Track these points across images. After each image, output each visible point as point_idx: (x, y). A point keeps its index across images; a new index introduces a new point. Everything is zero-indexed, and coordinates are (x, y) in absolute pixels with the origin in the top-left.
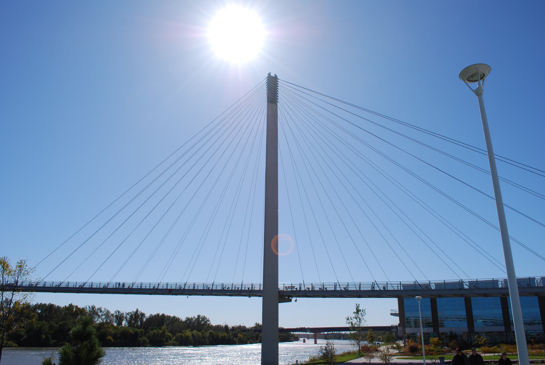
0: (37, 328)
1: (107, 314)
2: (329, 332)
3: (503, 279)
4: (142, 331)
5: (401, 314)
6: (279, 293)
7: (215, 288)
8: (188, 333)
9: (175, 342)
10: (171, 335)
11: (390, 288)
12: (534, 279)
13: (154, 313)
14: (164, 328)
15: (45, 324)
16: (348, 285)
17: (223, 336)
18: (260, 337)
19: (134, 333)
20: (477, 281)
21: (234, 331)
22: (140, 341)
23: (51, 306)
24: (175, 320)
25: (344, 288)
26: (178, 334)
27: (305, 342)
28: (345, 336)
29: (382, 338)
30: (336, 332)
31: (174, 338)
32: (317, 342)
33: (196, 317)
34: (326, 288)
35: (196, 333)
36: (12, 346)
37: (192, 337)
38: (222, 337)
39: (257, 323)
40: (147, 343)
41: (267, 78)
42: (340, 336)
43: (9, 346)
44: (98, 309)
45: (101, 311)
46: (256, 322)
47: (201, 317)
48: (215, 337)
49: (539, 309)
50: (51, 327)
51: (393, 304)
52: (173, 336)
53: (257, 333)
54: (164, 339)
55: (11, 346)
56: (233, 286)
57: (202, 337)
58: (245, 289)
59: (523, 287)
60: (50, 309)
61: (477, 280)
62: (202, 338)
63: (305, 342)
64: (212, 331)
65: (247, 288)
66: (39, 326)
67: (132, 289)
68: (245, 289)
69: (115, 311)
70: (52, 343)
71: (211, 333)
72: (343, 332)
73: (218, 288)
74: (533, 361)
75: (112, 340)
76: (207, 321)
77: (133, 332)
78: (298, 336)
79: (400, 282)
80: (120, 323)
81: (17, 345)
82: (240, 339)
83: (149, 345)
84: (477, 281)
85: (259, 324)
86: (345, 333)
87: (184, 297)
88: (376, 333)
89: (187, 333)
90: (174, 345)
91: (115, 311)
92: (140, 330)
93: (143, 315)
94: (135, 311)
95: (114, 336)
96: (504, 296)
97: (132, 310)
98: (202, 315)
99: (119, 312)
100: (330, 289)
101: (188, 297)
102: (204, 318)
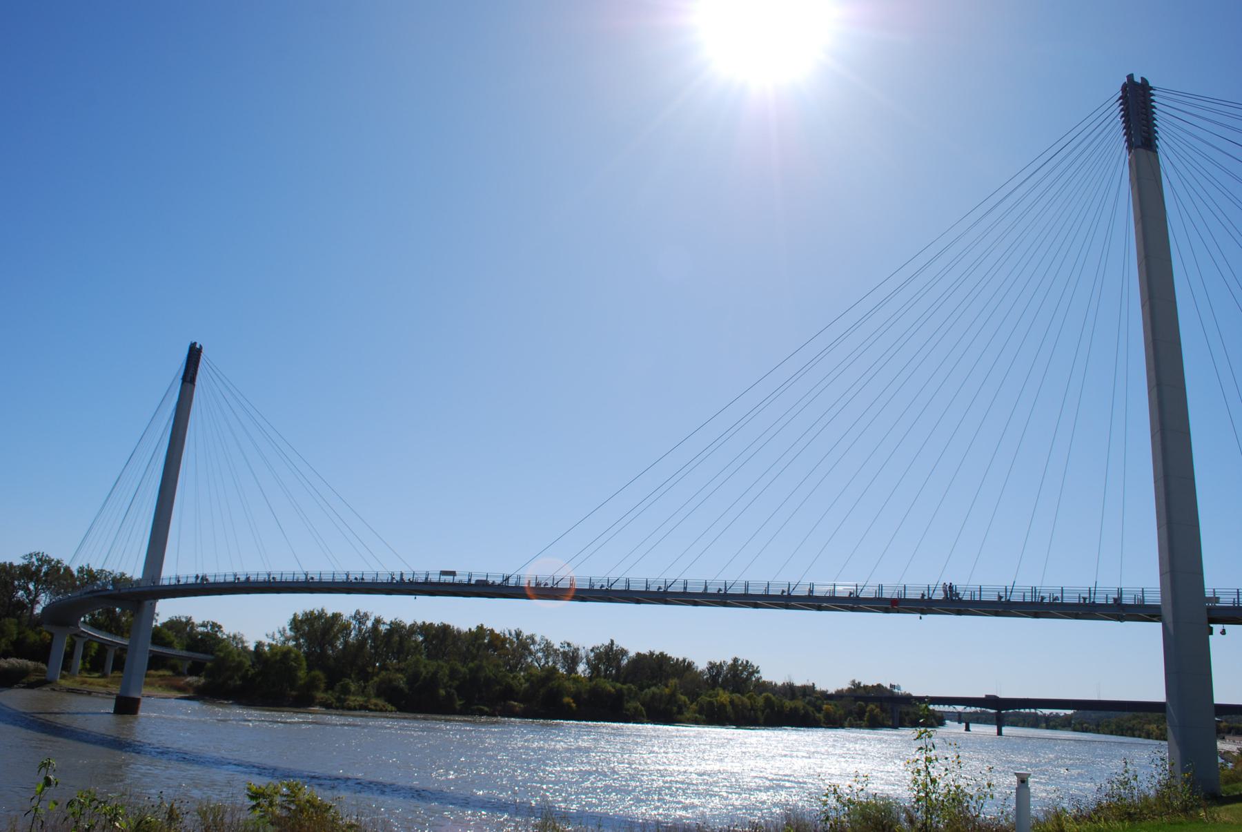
0: (427, 673)
1: (548, 649)
4: (629, 689)
6: (1208, 614)
7: (1018, 596)
8: (724, 697)
9: (697, 715)
10: (687, 700)
13: (645, 651)
14: (673, 684)
15: (442, 667)
16: (980, 591)
17: (793, 706)
19: (615, 693)
21: (808, 698)
22: (628, 710)
23: (445, 630)
24: (684, 668)
25: (1115, 599)
26: (704, 699)
27: (969, 731)
28: (1051, 721)
29: (1157, 731)
30: (1027, 710)
31: (694, 706)
32: (1003, 732)
33: (730, 662)
34: (239, 579)
35: (739, 698)
36: (386, 711)
37: (731, 707)
38: (791, 709)
39: (854, 681)
40: (643, 716)
41: (1120, 98)
42: (1037, 719)
43: (381, 710)
44: (528, 638)
45: (534, 642)
46: (852, 679)
47: (740, 662)
48: (776, 709)
50: (453, 673)
52: (691, 703)
53: (862, 703)
54: (675, 709)
55: (384, 709)
57: (750, 707)
58: (1107, 601)
60: (440, 636)
62: (751, 710)
64: (770, 695)
65: (1112, 600)
66: (432, 670)
67: (726, 595)
68: (1107, 601)
69: (561, 643)
70: (458, 707)
71: (767, 699)
72: (1047, 712)
75: (574, 705)
77: (613, 690)
78: (944, 715)
80: (572, 668)
81: (394, 708)
82: (827, 715)
83: (645, 720)
85: (859, 683)
86: (1051, 713)
87: (913, 618)
88: (1138, 717)
89: (721, 698)
90: (697, 722)
91: (561, 643)
92: (625, 687)
93: (624, 652)
94: (607, 643)
95: (576, 697)
96: (958, 610)
97: (602, 641)
98: (743, 657)
99: (569, 645)
101: (921, 618)
102: (747, 665)
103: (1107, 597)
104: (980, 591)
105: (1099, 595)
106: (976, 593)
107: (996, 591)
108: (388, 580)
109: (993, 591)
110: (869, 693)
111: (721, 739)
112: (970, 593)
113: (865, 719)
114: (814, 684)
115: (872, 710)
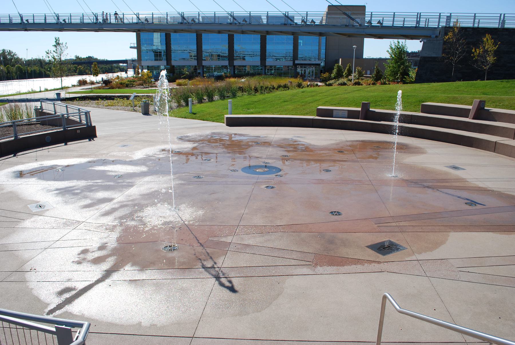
5: (139, 48)
11: (87, 20)
16: (71, 17)
18: (78, 70)
39: (76, 56)
48: (24, 71)
51: (131, 37)
59: (239, 23)
68: (393, 24)
71: (19, 67)
73: (408, 23)
76: (14, 55)
100: (38, 21)
102: (10, 53)
103: (404, 21)
104: (71, 17)
105: (7, 18)
106: (323, 18)
107: (320, 16)
108: (321, 22)
109: (412, 18)
110: (81, 61)
111: (424, 88)
112: (425, 20)
113: (77, 72)
114: (22, 58)
115: (80, 68)
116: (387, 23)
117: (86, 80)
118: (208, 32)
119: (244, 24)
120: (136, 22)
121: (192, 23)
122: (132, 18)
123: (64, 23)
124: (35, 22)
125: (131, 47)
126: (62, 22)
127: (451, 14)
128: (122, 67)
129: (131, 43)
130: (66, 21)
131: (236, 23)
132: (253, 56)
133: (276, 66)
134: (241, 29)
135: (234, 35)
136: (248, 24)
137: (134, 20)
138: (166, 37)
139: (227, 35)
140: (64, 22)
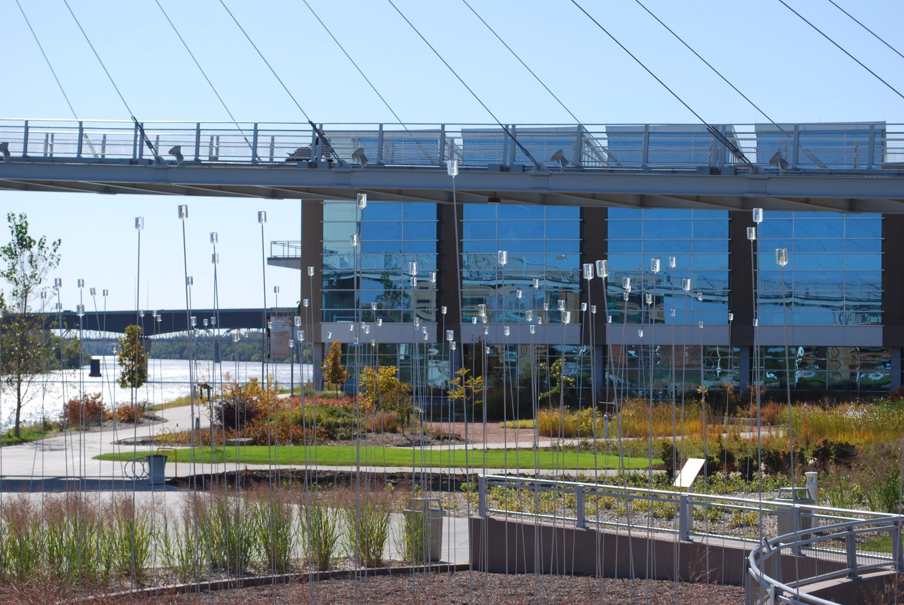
2: (233, 327)
3: (459, 128)
11: (232, 152)
12: (579, 134)
20: (381, 132)
27: (100, 375)
49: (880, 257)
56: (205, 139)
61: (381, 125)
63: (100, 375)
74: (282, 471)
79: (256, 125)
84: (381, 132)
116: (65, 150)
117: (98, 400)
118: (518, 202)
119: (557, 169)
120: (131, 157)
121: (357, 166)
122: (104, 141)
123: (172, 162)
124: (28, 154)
125: (274, 261)
126: (165, 158)
127: (443, 126)
128: (70, 346)
129: (275, 243)
130: (183, 151)
131: (524, 166)
132: (796, 304)
133: (767, 347)
134: (348, 184)
135: (610, 210)
136: (370, 167)
137: (277, 153)
138: (439, 216)
139: (576, 211)
140: (174, 158)
